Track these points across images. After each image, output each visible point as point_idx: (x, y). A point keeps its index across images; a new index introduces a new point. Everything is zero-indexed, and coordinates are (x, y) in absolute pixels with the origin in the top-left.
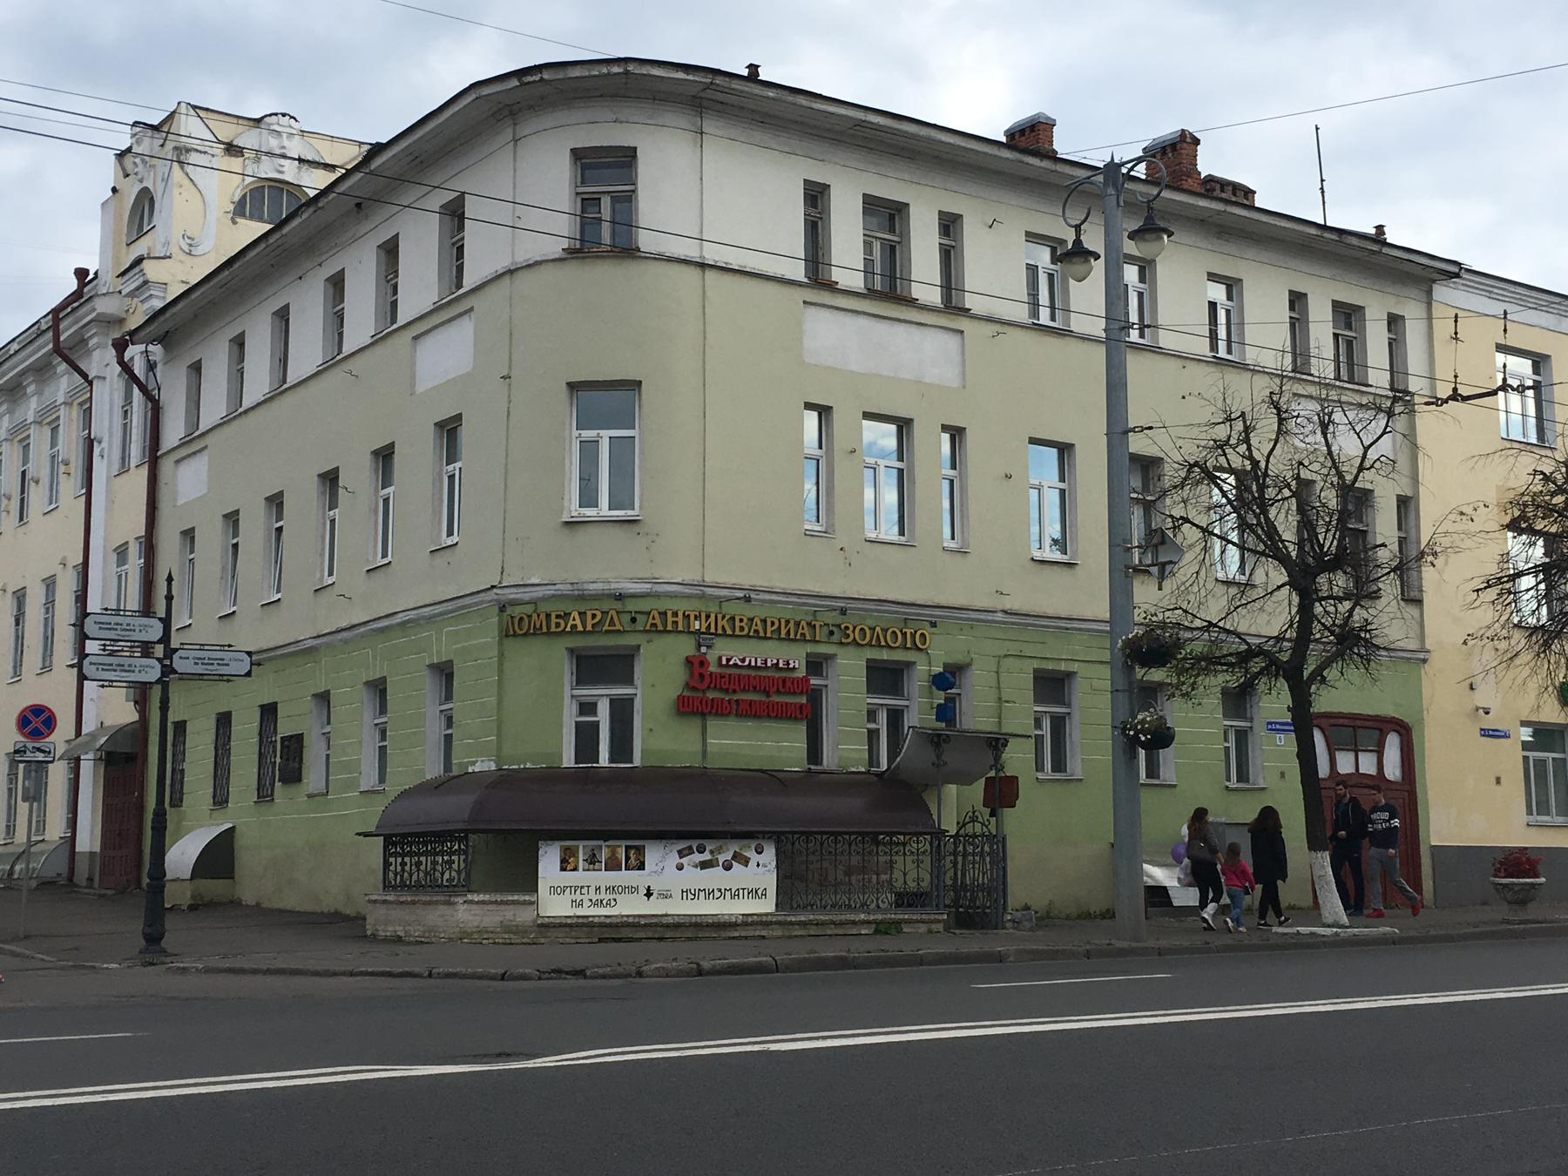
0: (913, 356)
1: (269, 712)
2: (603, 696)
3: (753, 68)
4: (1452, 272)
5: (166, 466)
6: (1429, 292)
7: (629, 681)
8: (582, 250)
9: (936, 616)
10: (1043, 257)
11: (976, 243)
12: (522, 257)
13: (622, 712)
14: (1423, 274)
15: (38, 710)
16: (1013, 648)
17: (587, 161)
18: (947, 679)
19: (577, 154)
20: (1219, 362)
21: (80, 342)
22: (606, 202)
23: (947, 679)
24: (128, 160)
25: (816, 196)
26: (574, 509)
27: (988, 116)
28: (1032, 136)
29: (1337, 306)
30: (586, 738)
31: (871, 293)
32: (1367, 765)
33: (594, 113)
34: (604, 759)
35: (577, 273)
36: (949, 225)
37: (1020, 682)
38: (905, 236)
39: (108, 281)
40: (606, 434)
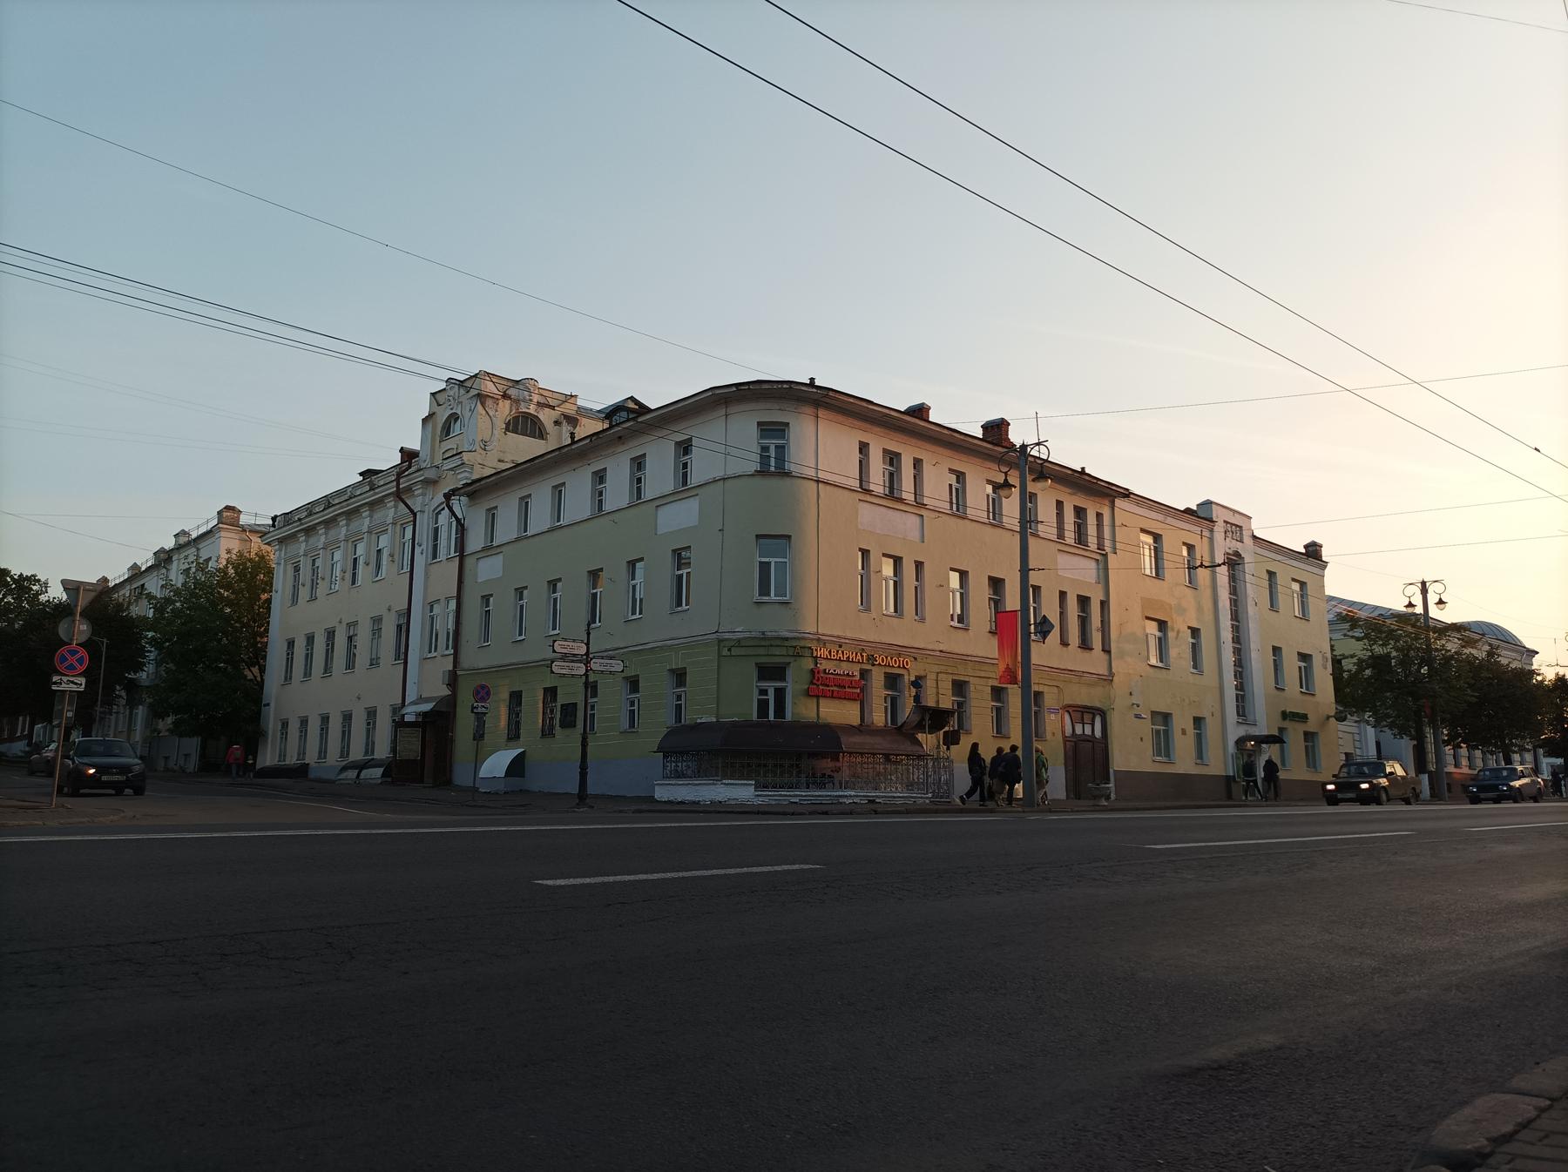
0: (900, 527)
1: (551, 693)
2: (771, 686)
3: (812, 379)
4: (1127, 494)
5: (469, 562)
6: (1113, 503)
7: (783, 679)
8: (763, 472)
9: (916, 653)
10: (989, 489)
11: (927, 468)
12: (730, 472)
13: (780, 693)
14: (1109, 493)
15: (483, 687)
16: (943, 668)
17: (767, 429)
18: (917, 683)
19: (759, 424)
20: (953, 515)
21: (409, 489)
22: (772, 448)
23: (917, 683)
24: (440, 398)
25: (864, 448)
26: (757, 597)
27: (900, 401)
28: (920, 411)
29: (1076, 507)
30: (763, 705)
31: (885, 497)
32: (1088, 731)
33: (777, 403)
34: (771, 717)
35: (758, 481)
36: (917, 463)
37: (946, 686)
38: (899, 469)
39: (424, 460)
40: (773, 560)
